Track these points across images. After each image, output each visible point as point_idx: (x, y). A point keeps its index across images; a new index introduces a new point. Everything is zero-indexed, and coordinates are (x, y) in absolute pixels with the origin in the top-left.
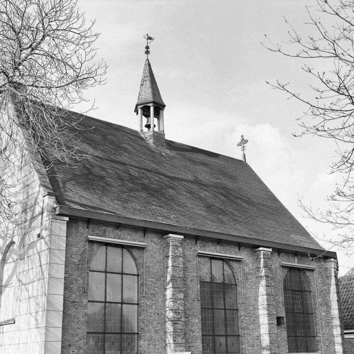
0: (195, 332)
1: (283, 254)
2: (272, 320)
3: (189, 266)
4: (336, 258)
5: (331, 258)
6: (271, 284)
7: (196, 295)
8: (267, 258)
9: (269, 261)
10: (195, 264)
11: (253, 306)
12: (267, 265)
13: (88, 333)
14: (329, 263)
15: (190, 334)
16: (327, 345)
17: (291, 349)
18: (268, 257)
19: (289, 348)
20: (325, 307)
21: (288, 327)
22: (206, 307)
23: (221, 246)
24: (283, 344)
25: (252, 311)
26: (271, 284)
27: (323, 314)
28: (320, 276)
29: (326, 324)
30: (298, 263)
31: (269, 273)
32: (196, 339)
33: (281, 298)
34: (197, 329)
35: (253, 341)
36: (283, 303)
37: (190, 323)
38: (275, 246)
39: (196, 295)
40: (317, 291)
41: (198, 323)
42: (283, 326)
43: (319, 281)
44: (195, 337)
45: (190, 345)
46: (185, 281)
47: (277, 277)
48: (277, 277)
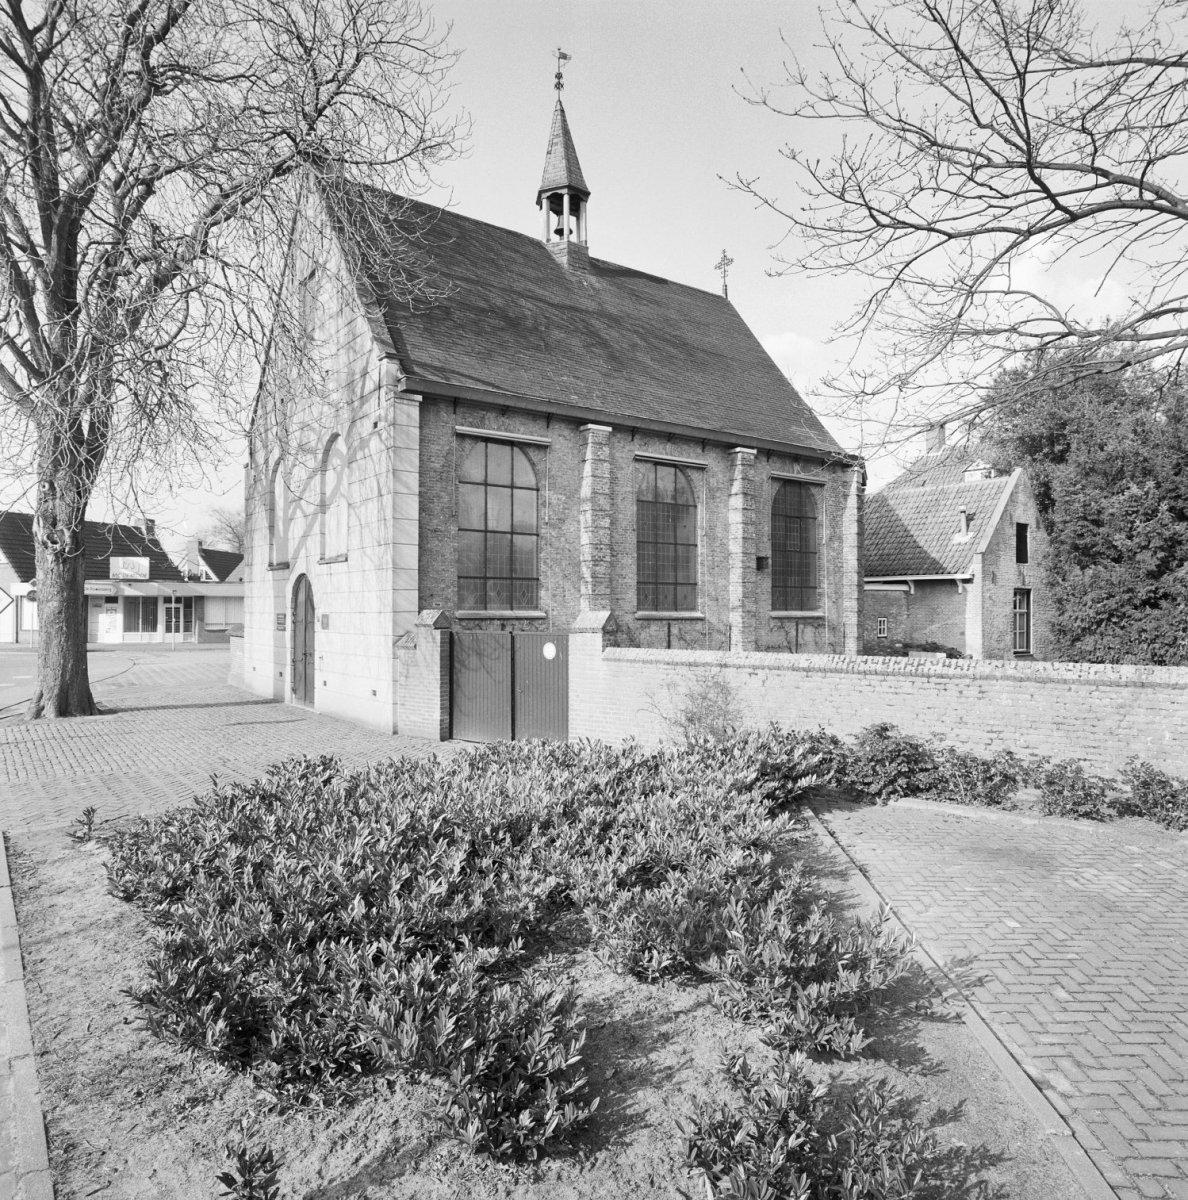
21: (774, 573)
38: (760, 445)
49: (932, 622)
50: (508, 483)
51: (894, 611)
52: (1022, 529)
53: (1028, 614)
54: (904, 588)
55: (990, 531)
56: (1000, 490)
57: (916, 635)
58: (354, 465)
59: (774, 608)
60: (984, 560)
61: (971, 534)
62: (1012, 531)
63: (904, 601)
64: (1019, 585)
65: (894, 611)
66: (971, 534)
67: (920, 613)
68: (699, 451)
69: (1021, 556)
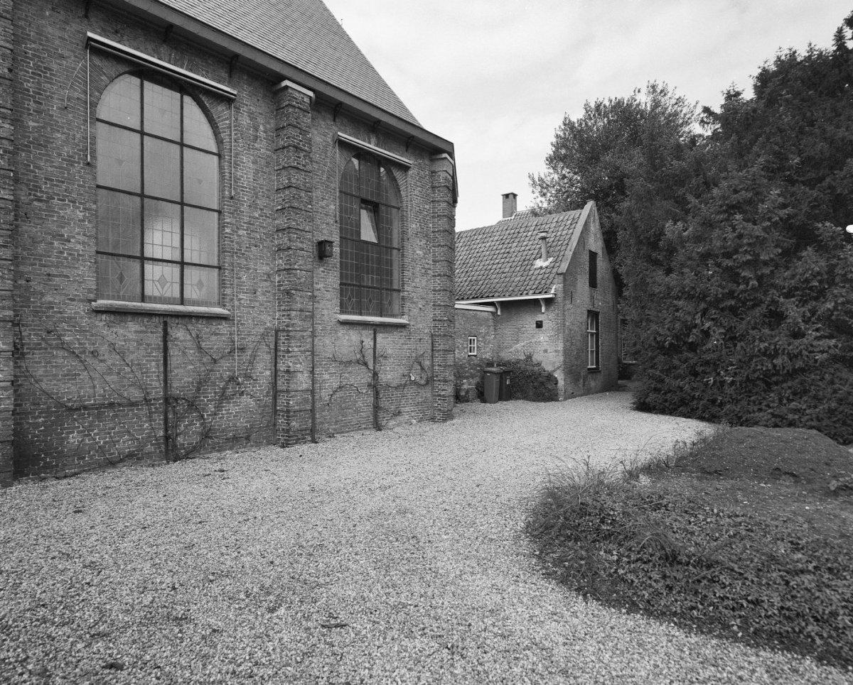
0: (72, 240)
1: (345, 121)
2: (302, 242)
3: (55, 67)
4: (451, 154)
5: (444, 151)
6: (304, 166)
7: (80, 150)
8: (299, 108)
9: (305, 116)
10: (81, 69)
11: (261, 210)
12: (297, 123)
13: (98, 252)
14: (440, 163)
15: (53, 244)
16: (421, 306)
17: (347, 308)
18: (301, 106)
19: (341, 306)
20: (424, 241)
21: (343, 266)
22: (349, 282)
23: (176, 48)
24: (328, 295)
25: (257, 218)
26: (304, 166)
27: (418, 252)
28: (419, 184)
29: (423, 271)
30: (377, 145)
31: (301, 141)
32: (73, 259)
33: (332, 207)
34: (78, 234)
35: (255, 283)
36: (335, 217)
37: (53, 216)
38: (321, 88)
39: (80, 150)
40: (411, 210)
41: (84, 221)
42: (331, 260)
43: (416, 192)
44: (70, 254)
45: (54, 271)
46: (41, 104)
47: (326, 162)
48: (326, 162)
49: (518, 341)
50: (177, 269)
51: (483, 330)
52: (593, 256)
53: (597, 334)
54: (491, 309)
55: (569, 254)
56: (575, 221)
57: (502, 354)
58: (292, 369)
59: (342, 312)
60: (565, 280)
61: (551, 259)
62: (586, 257)
63: (491, 323)
64: (590, 308)
65: (483, 330)
66: (551, 259)
67: (507, 330)
68: (224, 75)
69: (593, 283)
